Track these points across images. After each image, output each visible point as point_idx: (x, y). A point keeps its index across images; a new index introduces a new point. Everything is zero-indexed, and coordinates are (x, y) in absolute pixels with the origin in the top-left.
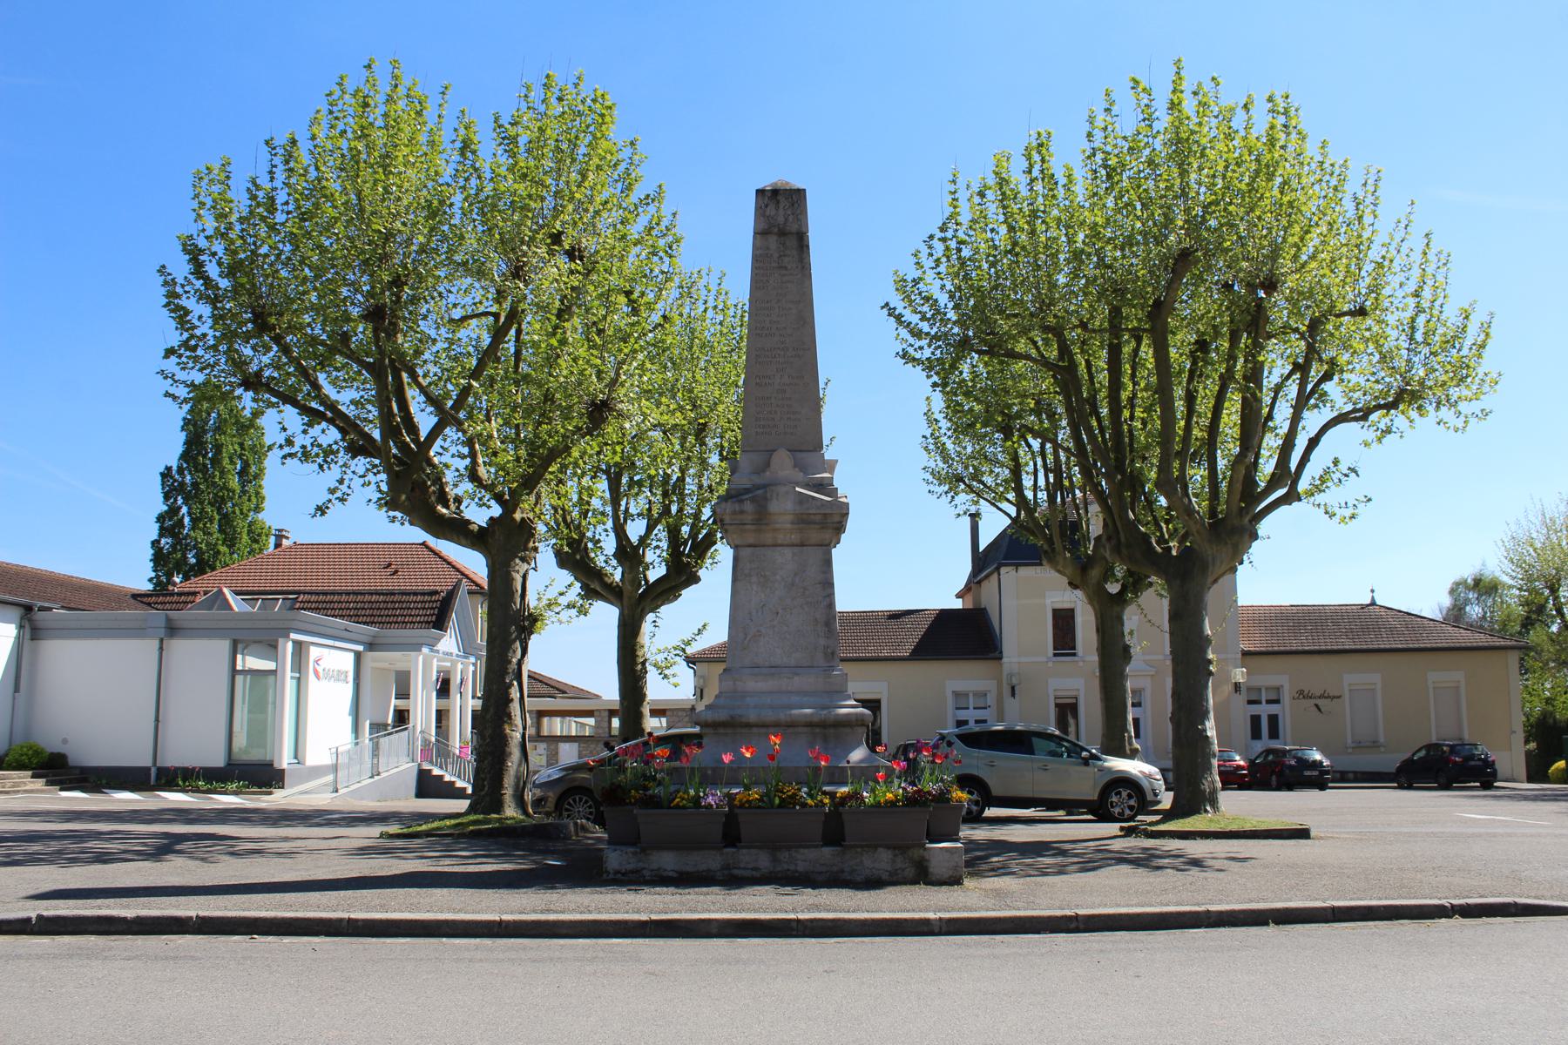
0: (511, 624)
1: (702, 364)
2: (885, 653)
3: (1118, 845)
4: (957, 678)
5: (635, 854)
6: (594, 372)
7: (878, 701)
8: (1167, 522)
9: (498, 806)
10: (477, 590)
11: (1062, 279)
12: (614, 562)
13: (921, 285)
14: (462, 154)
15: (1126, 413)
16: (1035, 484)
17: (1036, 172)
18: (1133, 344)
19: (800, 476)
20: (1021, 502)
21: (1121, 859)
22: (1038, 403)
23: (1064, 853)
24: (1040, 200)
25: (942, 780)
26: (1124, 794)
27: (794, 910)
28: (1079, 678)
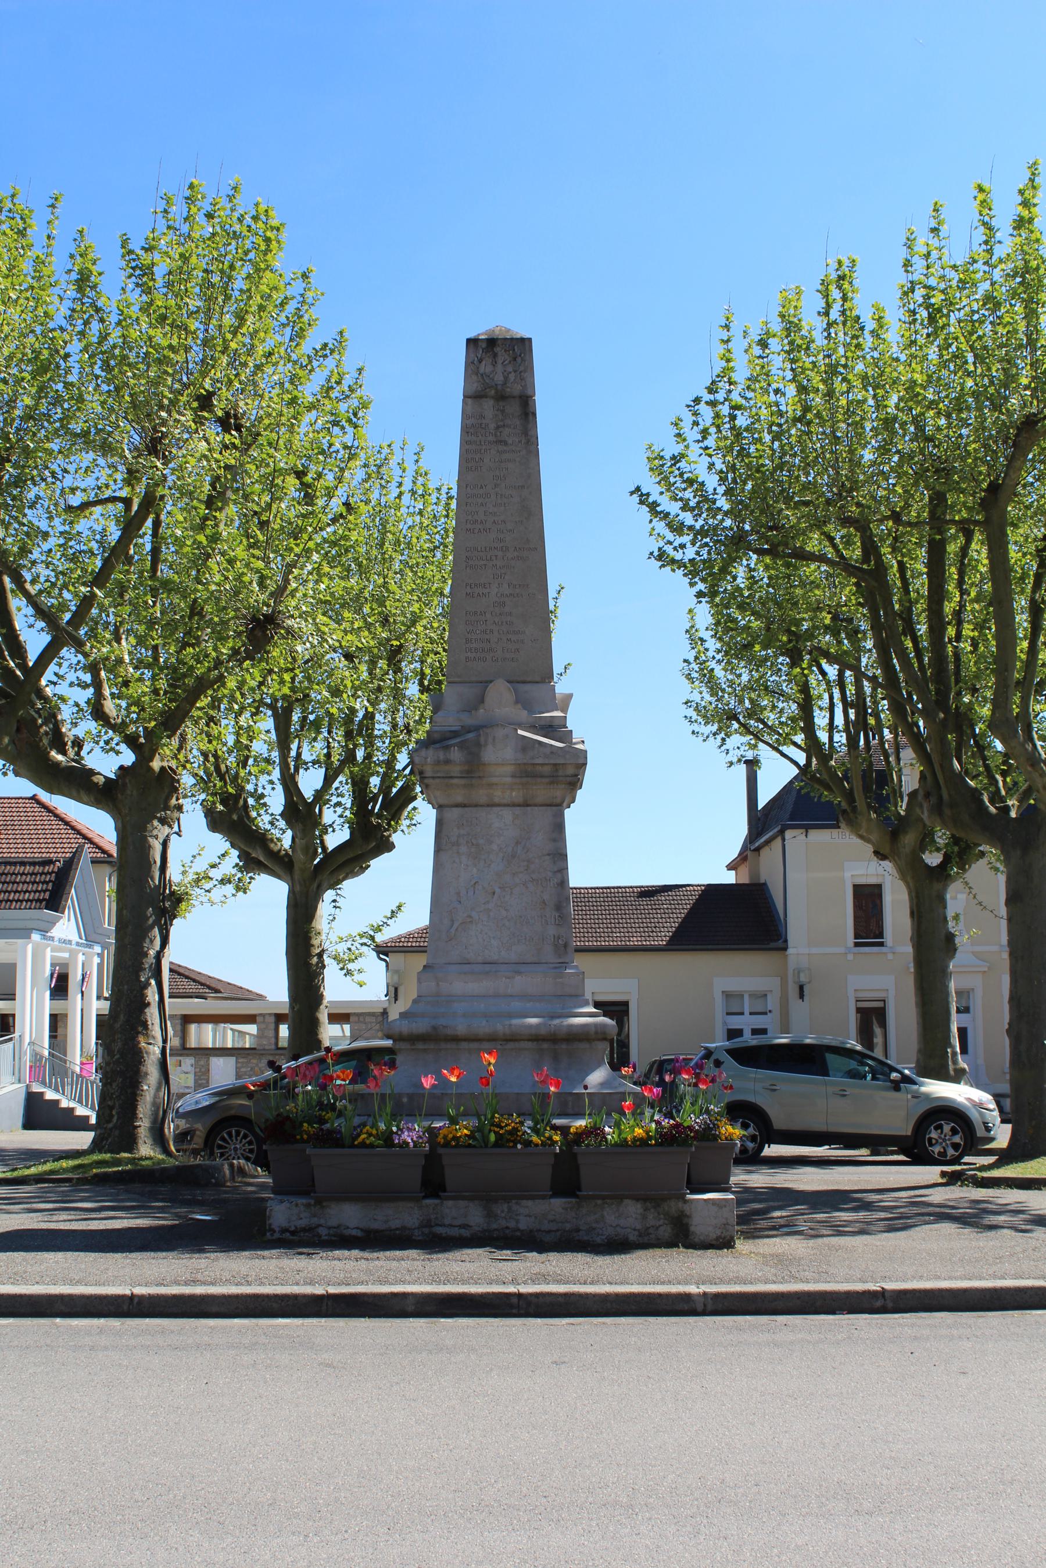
0: (147, 905)
1: (397, 566)
2: (635, 942)
3: (938, 1196)
4: (729, 975)
5: (308, 1206)
6: (256, 577)
7: (626, 1004)
8: (1004, 774)
9: (130, 1142)
10: (102, 859)
11: (868, 455)
12: (282, 824)
13: (682, 464)
14: (80, 290)
15: (951, 631)
16: (831, 722)
17: (835, 314)
18: (961, 540)
19: (523, 715)
20: (812, 746)
21: (943, 1215)
22: (835, 618)
23: (867, 1206)
24: (841, 350)
25: (708, 1112)
26: (947, 1128)
27: (514, 1281)
28: (888, 975)
